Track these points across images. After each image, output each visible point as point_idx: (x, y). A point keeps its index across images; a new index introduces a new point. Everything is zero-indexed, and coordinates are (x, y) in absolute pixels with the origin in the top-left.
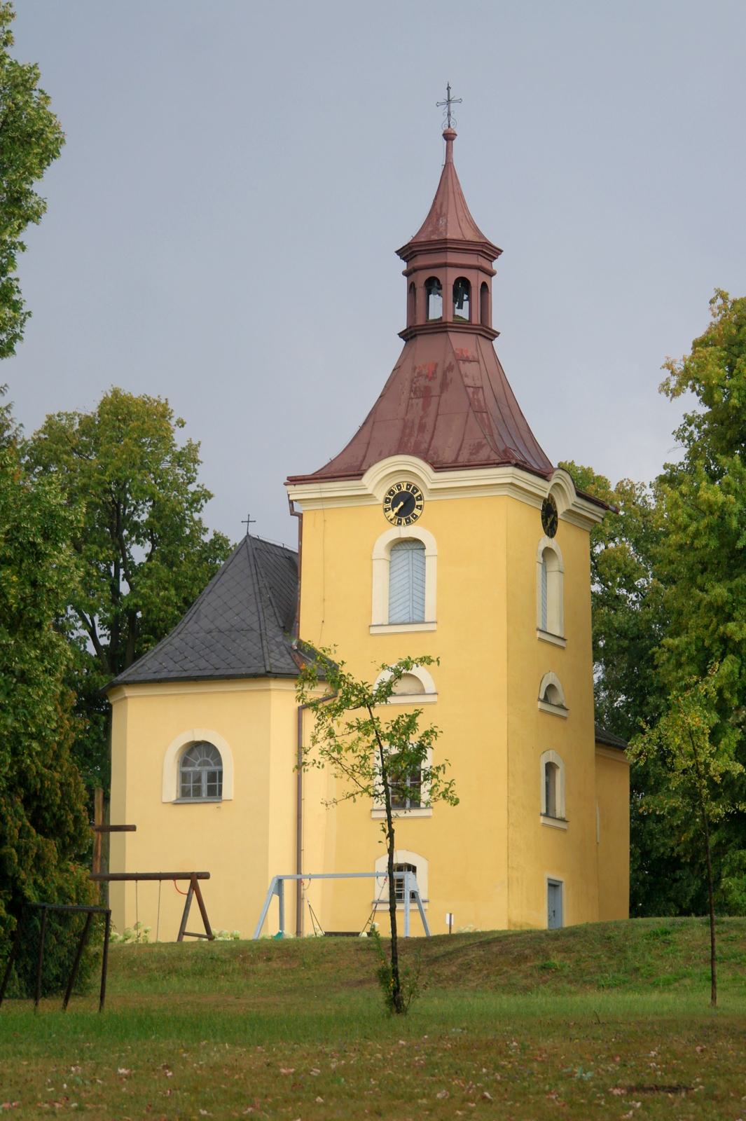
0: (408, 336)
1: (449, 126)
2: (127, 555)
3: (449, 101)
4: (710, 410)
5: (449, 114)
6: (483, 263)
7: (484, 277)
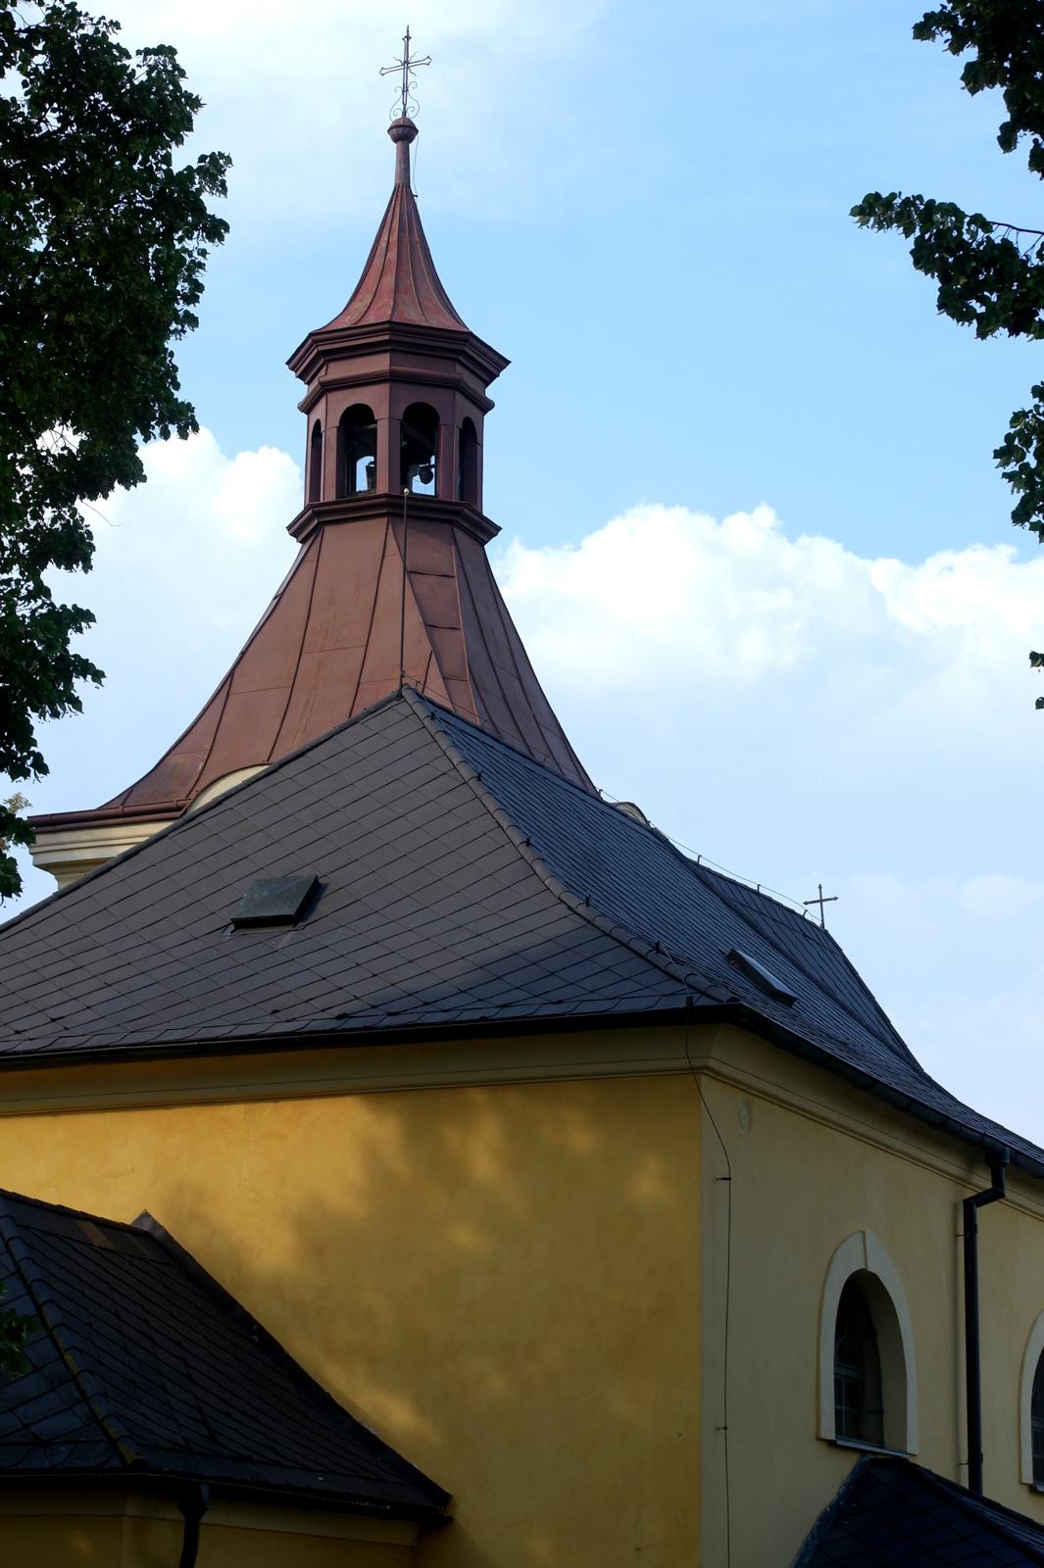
0: (308, 528)
1: (404, 113)
2: (59, 1467)
3: (406, 62)
4: (1005, 88)
5: (405, 90)
6: (470, 381)
7: (470, 410)
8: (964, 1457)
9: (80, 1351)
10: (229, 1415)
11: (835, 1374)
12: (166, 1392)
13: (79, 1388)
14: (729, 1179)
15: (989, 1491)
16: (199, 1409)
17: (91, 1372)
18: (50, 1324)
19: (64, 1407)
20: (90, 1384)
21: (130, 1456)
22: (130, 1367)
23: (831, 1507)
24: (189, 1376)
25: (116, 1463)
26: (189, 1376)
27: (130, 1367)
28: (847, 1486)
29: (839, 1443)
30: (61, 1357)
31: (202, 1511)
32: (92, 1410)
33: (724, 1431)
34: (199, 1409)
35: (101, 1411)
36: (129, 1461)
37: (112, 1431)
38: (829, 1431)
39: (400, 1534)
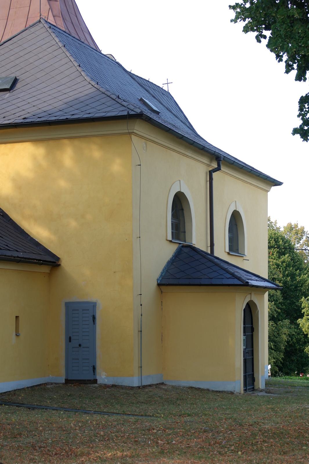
8: (209, 245)
15: (216, 254)
28: (175, 253)
38: (170, 238)
39: (45, 269)
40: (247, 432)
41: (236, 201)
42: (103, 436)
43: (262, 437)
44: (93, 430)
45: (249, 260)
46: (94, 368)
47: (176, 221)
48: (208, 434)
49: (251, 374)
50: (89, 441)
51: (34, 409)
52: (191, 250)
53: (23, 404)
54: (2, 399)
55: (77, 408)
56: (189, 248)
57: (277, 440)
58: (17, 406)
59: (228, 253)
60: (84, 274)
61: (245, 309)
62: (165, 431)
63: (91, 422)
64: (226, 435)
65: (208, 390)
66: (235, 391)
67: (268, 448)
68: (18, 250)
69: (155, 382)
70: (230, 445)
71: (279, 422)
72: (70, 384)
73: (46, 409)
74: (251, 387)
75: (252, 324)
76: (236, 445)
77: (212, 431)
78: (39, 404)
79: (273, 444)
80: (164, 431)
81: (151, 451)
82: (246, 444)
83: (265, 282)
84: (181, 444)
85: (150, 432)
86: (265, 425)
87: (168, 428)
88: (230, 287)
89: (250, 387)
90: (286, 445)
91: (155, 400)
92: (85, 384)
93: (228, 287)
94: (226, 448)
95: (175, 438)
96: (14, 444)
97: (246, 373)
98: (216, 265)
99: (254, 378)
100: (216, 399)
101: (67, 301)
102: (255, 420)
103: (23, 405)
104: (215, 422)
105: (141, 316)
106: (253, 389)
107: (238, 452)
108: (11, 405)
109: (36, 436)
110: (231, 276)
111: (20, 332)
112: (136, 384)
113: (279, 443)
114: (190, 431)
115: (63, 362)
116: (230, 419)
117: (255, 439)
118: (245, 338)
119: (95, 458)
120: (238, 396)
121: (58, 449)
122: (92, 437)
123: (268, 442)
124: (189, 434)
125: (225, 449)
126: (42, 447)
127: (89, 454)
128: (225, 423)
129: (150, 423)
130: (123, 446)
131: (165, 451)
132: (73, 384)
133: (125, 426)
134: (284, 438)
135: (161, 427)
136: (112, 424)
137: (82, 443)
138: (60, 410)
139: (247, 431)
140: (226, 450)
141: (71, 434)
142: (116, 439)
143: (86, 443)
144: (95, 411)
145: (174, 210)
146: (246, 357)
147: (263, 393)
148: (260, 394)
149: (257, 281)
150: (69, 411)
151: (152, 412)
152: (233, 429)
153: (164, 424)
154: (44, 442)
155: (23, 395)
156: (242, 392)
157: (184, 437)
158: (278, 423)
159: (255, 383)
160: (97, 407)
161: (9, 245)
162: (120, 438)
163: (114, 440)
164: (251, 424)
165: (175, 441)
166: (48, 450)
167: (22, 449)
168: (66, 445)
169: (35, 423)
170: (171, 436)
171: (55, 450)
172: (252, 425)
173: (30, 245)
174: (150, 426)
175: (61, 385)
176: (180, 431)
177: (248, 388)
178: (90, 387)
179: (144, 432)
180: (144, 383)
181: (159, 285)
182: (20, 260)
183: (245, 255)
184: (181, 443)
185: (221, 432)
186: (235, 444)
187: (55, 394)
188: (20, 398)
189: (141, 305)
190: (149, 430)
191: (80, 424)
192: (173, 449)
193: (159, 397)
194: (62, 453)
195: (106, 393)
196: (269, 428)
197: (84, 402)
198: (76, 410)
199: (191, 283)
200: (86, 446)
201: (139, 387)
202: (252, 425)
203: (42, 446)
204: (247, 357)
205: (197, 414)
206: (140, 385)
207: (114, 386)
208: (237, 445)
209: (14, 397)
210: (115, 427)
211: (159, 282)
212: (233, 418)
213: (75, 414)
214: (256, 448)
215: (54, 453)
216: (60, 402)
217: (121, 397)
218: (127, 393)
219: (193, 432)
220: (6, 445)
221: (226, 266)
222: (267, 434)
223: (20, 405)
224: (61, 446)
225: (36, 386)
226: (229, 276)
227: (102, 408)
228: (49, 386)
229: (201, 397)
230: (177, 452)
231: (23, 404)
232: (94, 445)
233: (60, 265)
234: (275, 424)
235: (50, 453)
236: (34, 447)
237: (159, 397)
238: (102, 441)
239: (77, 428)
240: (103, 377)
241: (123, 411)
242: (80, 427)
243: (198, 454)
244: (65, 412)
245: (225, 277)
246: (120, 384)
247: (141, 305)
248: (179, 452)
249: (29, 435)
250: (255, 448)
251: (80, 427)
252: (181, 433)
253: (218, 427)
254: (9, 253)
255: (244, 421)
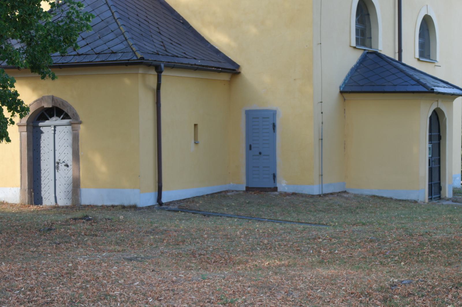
8: (397, 50)
9: (125, 26)
10: (172, 44)
11: (356, 27)
12: (152, 37)
13: (124, 36)
14: (322, 102)
15: (404, 61)
16: (162, 42)
17: (128, 32)
18: (116, 18)
19: (120, 42)
20: (127, 35)
21: (139, 56)
22: (141, 30)
23: (355, 66)
24: (160, 33)
25: (135, 58)
26: (160, 33)
27: (141, 30)
28: (360, 60)
29: (357, 47)
30: (119, 28)
31: (161, 72)
32: (128, 43)
33: (320, 45)
34: (162, 42)
35: (131, 42)
36: (139, 57)
37: (134, 49)
38: (354, 44)
39: (225, 77)
40: (415, 243)
41: (427, 5)
42: (266, 244)
43: (430, 247)
44: (257, 238)
45: (440, 66)
46: (274, 176)
47: (361, 27)
48: (375, 244)
49: (437, 183)
50: (251, 250)
51: (209, 216)
52: (376, 56)
53: (199, 211)
54: (180, 206)
55: (253, 215)
56: (374, 55)
57: (445, 251)
58: (193, 213)
59: (418, 60)
60: (264, 82)
61: (431, 116)
62: (331, 240)
63: (258, 230)
64: (392, 245)
65: (391, 199)
66: (418, 200)
67: (433, 259)
68: (197, 58)
69: (338, 191)
70: (394, 255)
71: (452, 232)
72: (251, 192)
73: (221, 216)
74: (437, 196)
75: (439, 131)
76: (401, 255)
77: (379, 241)
78: (215, 211)
79: (440, 255)
80: (329, 241)
81: (310, 260)
82: (412, 255)
83: (453, 88)
84: (344, 254)
85: (316, 240)
86: (437, 235)
87: (335, 238)
88: (415, 94)
89: (436, 196)
90: (454, 256)
91: (333, 209)
92: (266, 192)
93: (412, 94)
94: (390, 258)
95: (339, 247)
96: (174, 251)
97: (431, 181)
98: (402, 71)
99: (441, 187)
100: (397, 208)
101: (248, 109)
102: (427, 230)
103: (199, 212)
104: (384, 232)
105: (322, 124)
106: (440, 198)
107: (401, 262)
108: (187, 212)
109: (198, 243)
110: (416, 83)
111: (199, 140)
112: (316, 191)
113: (446, 254)
114: (356, 241)
115: (243, 170)
116: (402, 229)
117: (422, 249)
118: (431, 146)
119: (252, 267)
120: (421, 205)
121: (217, 257)
122: (254, 246)
123: (435, 253)
124: (354, 243)
125: (388, 260)
126: (202, 255)
127: (247, 262)
128: (395, 232)
129: (317, 232)
130: (283, 255)
131: (325, 261)
132: (253, 191)
133: (292, 235)
134: (453, 249)
135: (328, 236)
136: (278, 233)
137: (243, 252)
138: (234, 218)
139: (415, 241)
140: (389, 261)
141: (234, 242)
142: (278, 248)
143: (247, 251)
144: (269, 219)
145: (359, 16)
146: (432, 166)
147: (450, 203)
148: (445, 203)
149: (444, 88)
150: (243, 219)
151: (327, 220)
152: (401, 239)
153: (331, 233)
154: (205, 249)
155: (201, 202)
156: (427, 201)
157: (349, 247)
158: (450, 233)
159: (442, 192)
160: (273, 215)
161: (187, 53)
162: (282, 247)
163: (276, 248)
164: (422, 234)
165: (338, 250)
166: (208, 258)
167: (181, 257)
168: (226, 253)
169: (202, 230)
170: (335, 245)
171: (214, 258)
172: (422, 235)
173: (210, 52)
174: (316, 235)
175: (241, 192)
176: (345, 241)
177: (433, 197)
178: (270, 195)
179: (308, 241)
180: (326, 191)
181: (342, 92)
182: (197, 68)
183: (437, 61)
184: (344, 252)
185: (388, 242)
186: (400, 254)
187: (234, 201)
188: (198, 205)
189: (322, 113)
190: (315, 239)
191: (246, 232)
192: (334, 258)
193: (339, 205)
194: (221, 261)
195: (285, 201)
196: (440, 239)
197: (261, 209)
198: (250, 217)
199: (374, 90)
200: (246, 254)
201: (320, 195)
202: (422, 235)
203: (202, 253)
204: (433, 165)
205: (371, 223)
206: (321, 193)
207: (294, 194)
208: (402, 255)
209: (192, 204)
210: (280, 235)
211: (342, 89)
212: (404, 228)
213: (248, 222)
214: (421, 259)
215: (213, 260)
216: (237, 210)
217: (300, 205)
218: (306, 202)
219: (359, 241)
220: (166, 252)
221: (411, 73)
222: (435, 245)
223: (195, 212)
224: (221, 254)
225: (216, 193)
226: (415, 83)
227: (278, 216)
228: (229, 194)
229: (382, 206)
230: (338, 262)
231: (199, 211)
232: (255, 253)
233: (239, 73)
234: (447, 235)
235: (209, 261)
236: (193, 254)
237: (339, 205)
238: (264, 249)
239: (243, 236)
240: (284, 185)
241: (298, 220)
242: (245, 235)
243: (358, 264)
244: (239, 219)
245: (409, 84)
246: (300, 192)
247: (322, 113)
248: (340, 262)
249: (192, 243)
250: (420, 259)
251: (245, 235)
252: (346, 243)
253: (386, 236)
254: (186, 61)
255: (415, 231)
